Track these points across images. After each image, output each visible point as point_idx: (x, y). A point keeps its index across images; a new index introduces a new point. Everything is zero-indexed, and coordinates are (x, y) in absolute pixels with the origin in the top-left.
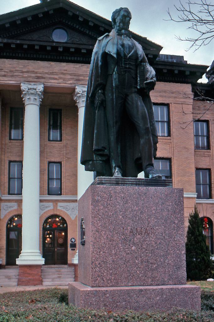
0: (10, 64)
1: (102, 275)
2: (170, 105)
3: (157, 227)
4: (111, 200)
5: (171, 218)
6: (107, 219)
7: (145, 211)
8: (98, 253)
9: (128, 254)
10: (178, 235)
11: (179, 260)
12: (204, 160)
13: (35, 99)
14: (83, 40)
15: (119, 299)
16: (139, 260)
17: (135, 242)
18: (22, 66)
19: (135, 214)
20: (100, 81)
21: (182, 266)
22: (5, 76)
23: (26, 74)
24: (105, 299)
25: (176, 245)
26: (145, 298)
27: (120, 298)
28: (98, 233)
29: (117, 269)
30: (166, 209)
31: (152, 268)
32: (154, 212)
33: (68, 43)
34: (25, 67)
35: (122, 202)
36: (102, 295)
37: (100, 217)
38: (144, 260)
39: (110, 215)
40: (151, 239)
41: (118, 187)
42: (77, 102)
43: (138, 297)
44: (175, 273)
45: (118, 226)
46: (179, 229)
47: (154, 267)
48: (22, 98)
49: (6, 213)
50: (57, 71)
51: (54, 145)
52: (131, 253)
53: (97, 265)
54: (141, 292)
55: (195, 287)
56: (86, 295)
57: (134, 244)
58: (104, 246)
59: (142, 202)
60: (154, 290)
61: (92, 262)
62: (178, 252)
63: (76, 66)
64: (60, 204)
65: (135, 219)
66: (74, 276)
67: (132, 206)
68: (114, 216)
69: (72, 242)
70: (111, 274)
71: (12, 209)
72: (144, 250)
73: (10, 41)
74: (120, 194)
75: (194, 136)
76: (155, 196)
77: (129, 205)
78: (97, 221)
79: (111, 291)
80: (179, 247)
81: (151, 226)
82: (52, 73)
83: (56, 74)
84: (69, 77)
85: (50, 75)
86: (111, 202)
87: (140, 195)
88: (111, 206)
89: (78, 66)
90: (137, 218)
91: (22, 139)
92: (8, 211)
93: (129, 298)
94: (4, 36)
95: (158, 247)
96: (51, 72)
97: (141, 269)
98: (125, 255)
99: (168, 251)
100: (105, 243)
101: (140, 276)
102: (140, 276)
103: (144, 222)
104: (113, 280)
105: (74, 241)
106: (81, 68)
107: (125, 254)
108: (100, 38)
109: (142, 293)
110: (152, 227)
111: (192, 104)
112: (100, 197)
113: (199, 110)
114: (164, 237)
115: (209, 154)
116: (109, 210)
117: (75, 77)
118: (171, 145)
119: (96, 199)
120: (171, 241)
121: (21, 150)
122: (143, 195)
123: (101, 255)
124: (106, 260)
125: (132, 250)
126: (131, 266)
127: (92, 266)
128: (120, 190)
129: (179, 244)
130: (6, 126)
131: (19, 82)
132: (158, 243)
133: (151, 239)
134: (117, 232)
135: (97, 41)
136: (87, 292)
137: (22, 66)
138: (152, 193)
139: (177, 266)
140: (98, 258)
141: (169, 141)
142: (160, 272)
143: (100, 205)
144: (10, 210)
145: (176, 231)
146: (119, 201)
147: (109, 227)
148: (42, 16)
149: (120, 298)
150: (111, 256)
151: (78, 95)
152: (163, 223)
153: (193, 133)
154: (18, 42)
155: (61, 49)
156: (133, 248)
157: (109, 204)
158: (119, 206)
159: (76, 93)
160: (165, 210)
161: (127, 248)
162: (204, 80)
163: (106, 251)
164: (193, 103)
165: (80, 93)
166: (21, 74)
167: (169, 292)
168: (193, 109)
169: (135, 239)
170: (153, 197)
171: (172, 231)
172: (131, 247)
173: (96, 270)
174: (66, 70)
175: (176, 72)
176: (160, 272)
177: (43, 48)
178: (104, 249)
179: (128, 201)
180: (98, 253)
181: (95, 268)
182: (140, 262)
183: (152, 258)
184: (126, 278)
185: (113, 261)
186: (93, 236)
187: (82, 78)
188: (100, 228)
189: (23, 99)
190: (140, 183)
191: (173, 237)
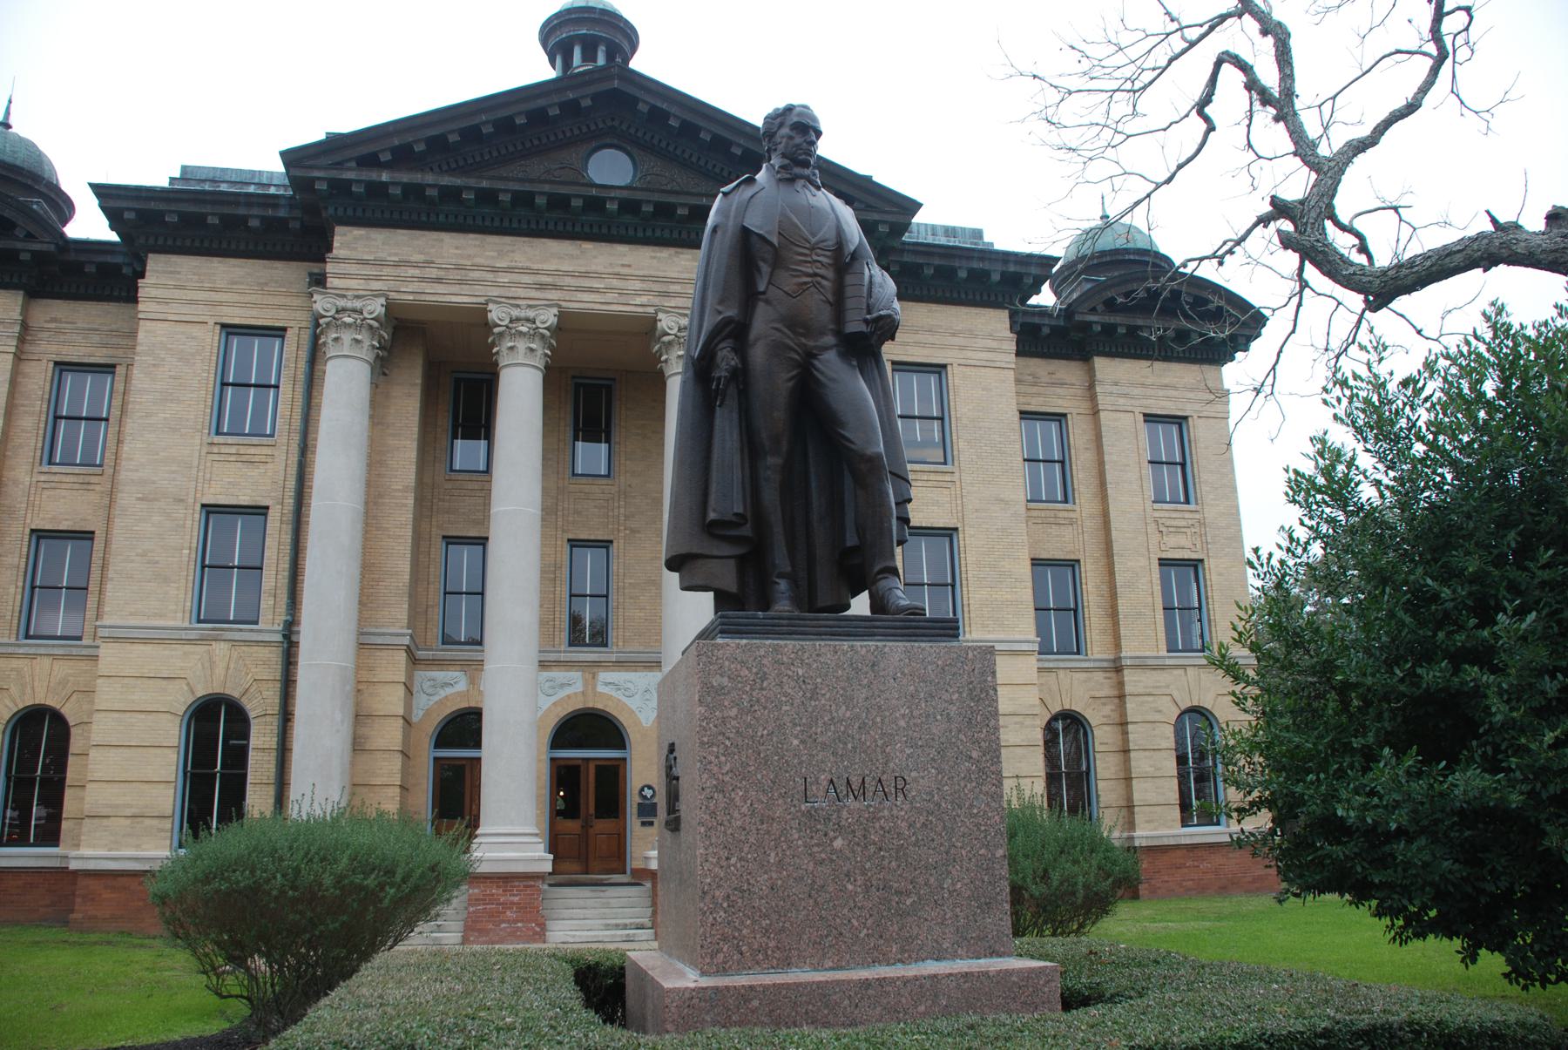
0: (457, 248)
1: (737, 934)
2: (1069, 416)
3: (914, 774)
4: (762, 689)
5: (959, 743)
6: (750, 751)
7: (874, 723)
8: (724, 863)
9: (822, 862)
10: (982, 796)
11: (986, 879)
12: (1057, 536)
13: (532, 350)
14: (679, 180)
15: (794, 1014)
16: (859, 883)
17: (843, 823)
18: (495, 254)
19: (843, 733)
20: (731, 312)
21: (999, 898)
22: (439, 280)
23: (505, 277)
24: (746, 1015)
25: (975, 829)
26: (879, 1009)
27: (797, 1012)
28: (721, 796)
29: (785, 916)
30: (941, 715)
31: (900, 909)
32: (902, 723)
33: (635, 189)
34: (501, 254)
35: (801, 693)
36: (737, 1003)
37: (727, 743)
38: (874, 883)
39: (762, 736)
40: (895, 812)
41: (786, 645)
42: (663, 358)
43: (857, 1006)
44: (976, 921)
45: (786, 771)
46: (984, 777)
47: (908, 903)
48: (493, 344)
49: (431, 703)
50: (600, 269)
51: (587, 488)
52: (832, 861)
53: (720, 901)
54: (867, 989)
55: (1040, 968)
56: (684, 1002)
57: (839, 828)
58: (743, 838)
59: (864, 693)
60: (908, 981)
61: (704, 893)
62: (982, 851)
63: (658, 255)
64: (604, 676)
65: (843, 748)
66: (651, 909)
67: (834, 707)
68: (775, 739)
69: (645, 797)
70: (767, 931)
71: (449, 691)
72: (872, 849)
73: (458, 181)
74: (792, 668)
75: (1025, 460)
76: (906, 671)
77: (823, 702)
78: (717, 757)
79: (766, 988)
80: (986, 837)
81: (894, 771)
82: (585, 275)
83: (598, 276)
84: (637, 285)
85: (580, 280)
86: (764, 693)
87: (857, 670)
88: (765, 708)
89: (665, 253)
90: (850, 746)
91: (488, 471)
92: (436, 698)
93: (826, 1012)
94: (441, 169)
95: (917, 840)
96: (583, 269)
97: (865, 913)
98: (811, 868)
99: (953, 851)
100: (744, 829)
101: (862, 935)
102: (862, 935)
103: (873, 756)
104: (773, 951)
105: (652, 796)
106: (675, 259)
107: (811, 864)
108: (725, 189)
109: (871, 992)
110: (897, 775)
111: (1013, 366)
112: (729, 677)
113: (1035, 384)
114: (938, 805)
115: (1072, 515)
116: (757, 720)
117: (663, 288)
118: (953, 489)
119: (715, 684)
120: (959, 816)
121: (485, 505)
122: (865, 669)
123: (732, 868)
124: (749, 884)
125: (833, 851)
126: (831, 904)
127: (702, 905)
128: (792, 656)
129: (986, 825)
130: (439, 430)
131: (482, 300)
132: (918, 825)
133: (895, 812)
134: (783, 791)
135: (720, 195)
136: (687, 995)
137: (492, 254)
138: (897, 664)
139: (983, 899)
140: (721, 879)
141: (948, 478)
142: (926, 920)
143: (726, 703)
144: (443, 693)
145: (974, 784)
146: (789, 691)
147: (759, 776)
148: (558, 112)
149: (797, 1012)
150: (766, 873)
151: (666, 339)
152: (933, 759)
153: (1019, 453)
154: (485, 184)
155: (612, 206)
156: (838, 843)
157: (758, 701)
158: (788, 708)
159: (657, 334)
160: (939, 717)
161: (818, 845)
162: (1045, 297)
163: (749, 856)
164: (1016, 363)
165: (669, 334)
166: (490, 276)
167: (958, 987)
168: (1018, 381)
169: (845, 814)
170: (899, 675)
171: (962, 784)
172: (832, 841)
173: (715, 919)
174: (629, 266)
175: (963, 274)
176: (926, 920)
177: (559, 203)
178: (741, 850)
179: (818, 690)
180: (724, 863)
181: (711, 913)
182: (859, 890)
183: (900, 875)
184: (815, 943)
185: (772, 889)
186: (704, 807)
187: (674, 288)
188: (727, 778)
189: (495, 350)
190: (860, 629)
191: (967, 804)
